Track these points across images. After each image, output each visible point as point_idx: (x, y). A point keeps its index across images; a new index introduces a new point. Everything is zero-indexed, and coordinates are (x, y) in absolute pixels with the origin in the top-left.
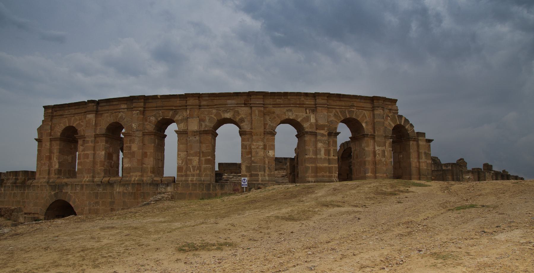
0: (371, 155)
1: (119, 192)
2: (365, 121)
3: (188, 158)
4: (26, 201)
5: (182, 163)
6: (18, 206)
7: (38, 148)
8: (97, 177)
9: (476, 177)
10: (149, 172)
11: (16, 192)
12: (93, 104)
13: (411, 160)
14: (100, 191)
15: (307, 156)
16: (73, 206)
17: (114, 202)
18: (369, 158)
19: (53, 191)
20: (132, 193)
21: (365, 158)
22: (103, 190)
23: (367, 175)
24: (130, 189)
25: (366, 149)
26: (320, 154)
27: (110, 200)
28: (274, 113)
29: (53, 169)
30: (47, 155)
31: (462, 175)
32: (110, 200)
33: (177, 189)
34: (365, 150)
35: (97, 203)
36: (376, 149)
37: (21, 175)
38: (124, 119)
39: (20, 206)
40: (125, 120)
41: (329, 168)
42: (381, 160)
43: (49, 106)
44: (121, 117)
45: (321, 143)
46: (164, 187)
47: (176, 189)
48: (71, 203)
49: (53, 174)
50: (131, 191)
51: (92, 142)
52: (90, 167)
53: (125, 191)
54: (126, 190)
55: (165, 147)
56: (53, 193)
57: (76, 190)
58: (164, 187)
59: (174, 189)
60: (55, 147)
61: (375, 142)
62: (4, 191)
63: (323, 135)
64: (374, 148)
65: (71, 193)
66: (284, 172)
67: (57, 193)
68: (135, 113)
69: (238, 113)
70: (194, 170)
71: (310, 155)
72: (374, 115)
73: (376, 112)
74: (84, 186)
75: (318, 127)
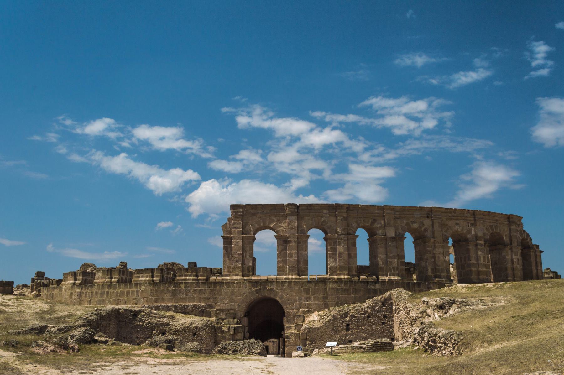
0: (510, 262)
1: (332, 288)
2: (505, 234)
3: (389, 260)
4: (217, 297)
5: (383, 264)
6: (208, 303)
7: (224, 244)
8: (114, 278)
9: (321, 302)
10: (354, 271)
11: (203, 288)
12: (294, 207)
13: (532, 267)
14: (312, 287)
15: (471, 262)
16: (280, 301)
17: (327, 297)
18: (509, 265)
19: (254, 288)
20: (345, 289)
21: (507, 264)
22: (315, 286)
23: (508, 278)
24: (343, 285)
25: (507, 257)
26: (481, 261)
27: (323, 295)
28: (447, 225)
29: (247, 267)
30: (239, 252)
31: (56, 311)
32: (323, 295)
33: (384, 286)
34: (506, 258)
35: (308, 299)
36: (514, 257)
37: (201, 271)
38: (327, 223)
39: (209, 303)
40: (328, 224)
41: (487, 271)
42: (517, 267)
43: (240, 205)
44: (324, 221)
45: (481, 251)
46: (373, 284)
47: (383, 287)
48: (277, 299)
49: (246, 271)
50: (344, 287)
51: (295, 242)
52: (294, 266)
53: (338, 287)
54: (339, 286)
55: (369, 251)
56: (254, 289)
57: (283, 286)
58: (373, 284)
59: (382, 286)
60: (248, 245)
61: (512, 251)
62: (185, 287)
63: (481, 245)
64: (512, 257)
65: (277, 289)
66: (147, 277)
67: (260, 289)
68: (339, 219)
69: (423, 224)
70: (394, 270)
71: (473, 261)
72: (510, 229)
73: (512, 227)
74: (293, 283)
75: (477, 238)
